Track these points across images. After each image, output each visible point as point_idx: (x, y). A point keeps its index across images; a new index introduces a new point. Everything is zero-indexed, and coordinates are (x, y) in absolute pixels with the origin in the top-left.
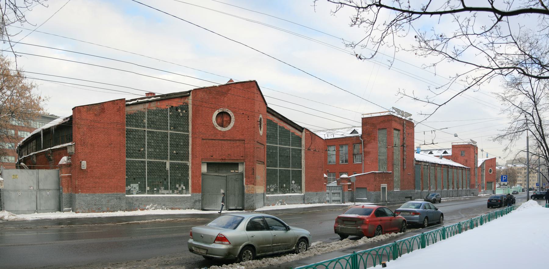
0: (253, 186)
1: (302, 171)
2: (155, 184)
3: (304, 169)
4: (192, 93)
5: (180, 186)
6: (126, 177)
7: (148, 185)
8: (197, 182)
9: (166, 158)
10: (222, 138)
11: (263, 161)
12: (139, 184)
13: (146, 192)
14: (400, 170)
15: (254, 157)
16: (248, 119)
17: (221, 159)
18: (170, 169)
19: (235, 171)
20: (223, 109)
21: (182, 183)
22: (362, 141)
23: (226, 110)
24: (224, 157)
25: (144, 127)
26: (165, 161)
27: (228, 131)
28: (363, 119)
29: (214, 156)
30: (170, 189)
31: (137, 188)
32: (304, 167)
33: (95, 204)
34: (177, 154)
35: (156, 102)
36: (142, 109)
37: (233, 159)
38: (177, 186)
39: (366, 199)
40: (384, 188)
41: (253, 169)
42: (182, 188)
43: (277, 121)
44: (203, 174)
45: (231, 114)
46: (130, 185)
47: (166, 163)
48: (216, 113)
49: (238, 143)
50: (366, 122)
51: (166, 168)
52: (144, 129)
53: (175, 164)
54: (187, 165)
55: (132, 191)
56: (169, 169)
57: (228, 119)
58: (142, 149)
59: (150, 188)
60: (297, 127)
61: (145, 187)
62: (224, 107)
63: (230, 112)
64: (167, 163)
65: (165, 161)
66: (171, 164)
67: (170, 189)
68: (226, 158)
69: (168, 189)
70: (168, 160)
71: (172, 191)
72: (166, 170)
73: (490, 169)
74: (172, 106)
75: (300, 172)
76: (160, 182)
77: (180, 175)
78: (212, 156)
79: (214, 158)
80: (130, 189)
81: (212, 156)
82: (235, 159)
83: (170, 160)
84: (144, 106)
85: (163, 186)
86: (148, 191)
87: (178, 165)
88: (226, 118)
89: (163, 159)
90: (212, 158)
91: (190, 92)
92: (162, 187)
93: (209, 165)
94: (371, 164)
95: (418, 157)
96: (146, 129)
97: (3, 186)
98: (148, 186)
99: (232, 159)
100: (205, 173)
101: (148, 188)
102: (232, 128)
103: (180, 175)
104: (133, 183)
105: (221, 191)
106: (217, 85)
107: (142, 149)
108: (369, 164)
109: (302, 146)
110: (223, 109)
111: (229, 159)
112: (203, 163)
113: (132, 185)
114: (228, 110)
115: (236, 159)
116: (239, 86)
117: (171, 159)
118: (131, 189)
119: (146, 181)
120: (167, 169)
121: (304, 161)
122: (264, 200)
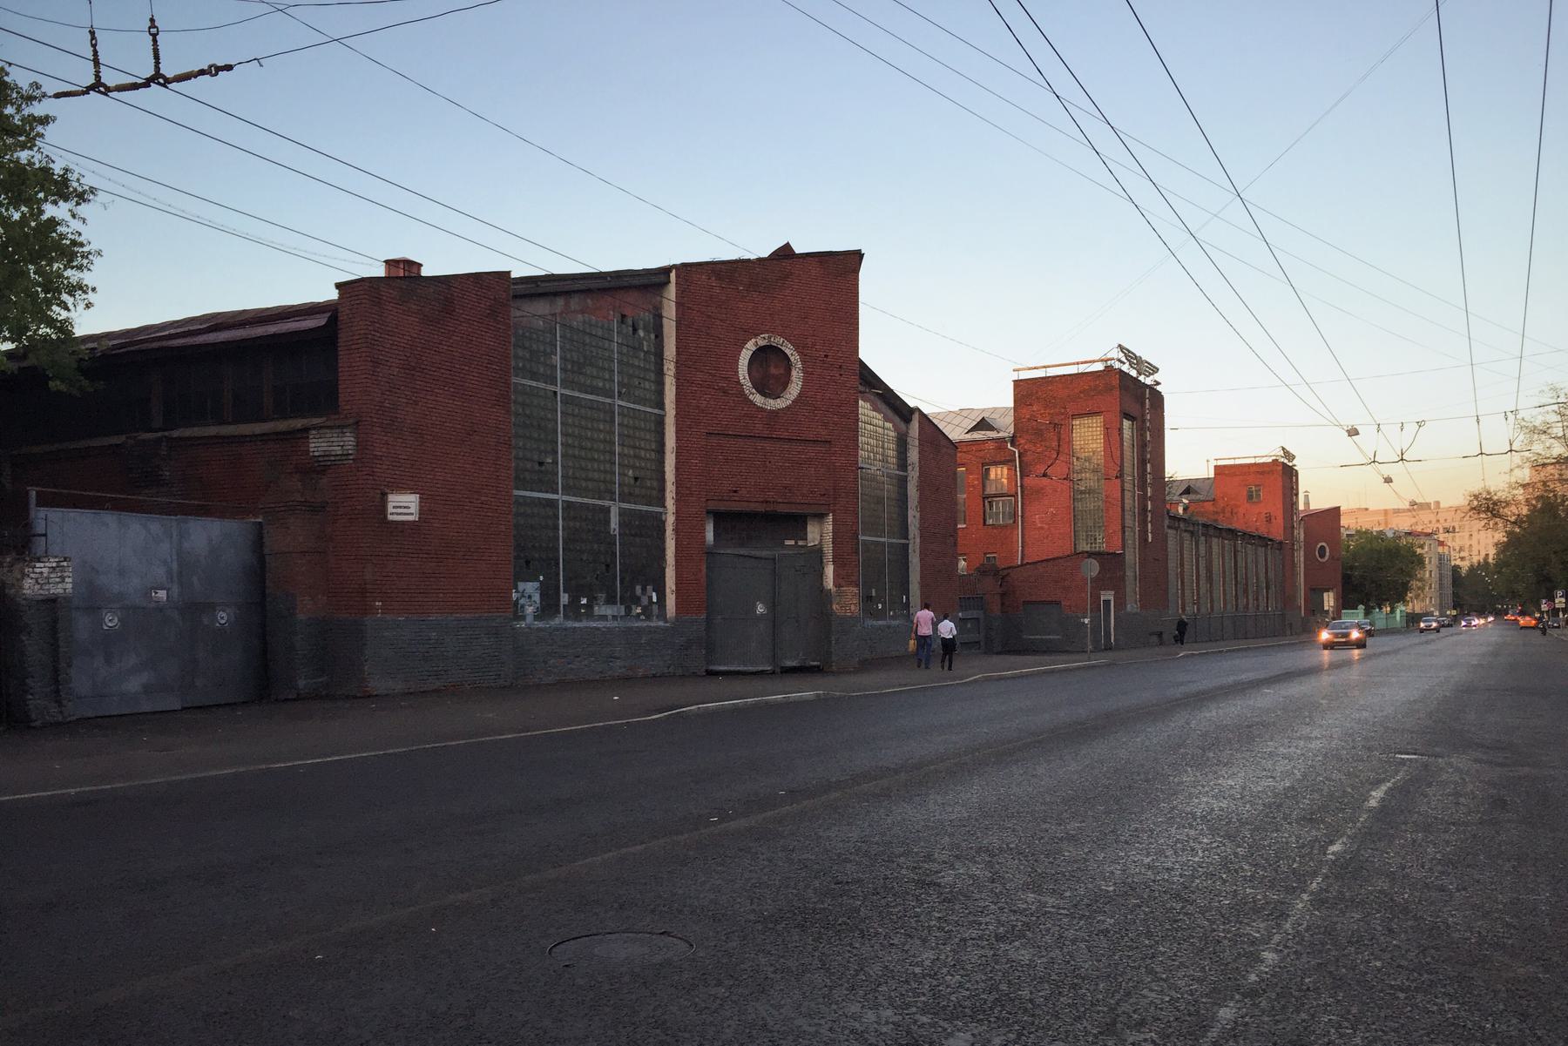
1: (910, 546)
3: (918, 540)
4: (677, 276)
5: (644, 590)
10: (766, 433)
14: (1137, 547)
17: (762, 502)
19: (796, 543)
20: (770, 337)
22: (1017, 455)
23: (778, 341)
25: (553, 381)
26: (607, 503)
28: (1017, 383)
29: (743, 492)
31: (537, 597)
32: (917, 533)
33: (426, 654)
40: (1107, 602)
44: (710, 553)
48: (750, 347)
50: (1026, 391)
52: (552, 388)
56: (617, 532)
57: (782, 371)
59: (569, 596)
62: (772, 331)
63: (789, 350)
65: (607, 503)
66: (622, 513)
67: (621, 604)
69: (614, 603)
73: (1322, 546)
78: (735, 492)
86: (564, 605)
88: (776, 367)
91: (666, 271)
94: (1046, 527)
95: (390, 518)
96: (559, 390)
97: (70, 586)
101: (564, 598)
106: (753, 257)
108: (1042, 528)
109: (910, 468)
110: (770, 337)
115: (806, 502)
118: (522, 601)
120: (612, 533)
121: (918, 515)
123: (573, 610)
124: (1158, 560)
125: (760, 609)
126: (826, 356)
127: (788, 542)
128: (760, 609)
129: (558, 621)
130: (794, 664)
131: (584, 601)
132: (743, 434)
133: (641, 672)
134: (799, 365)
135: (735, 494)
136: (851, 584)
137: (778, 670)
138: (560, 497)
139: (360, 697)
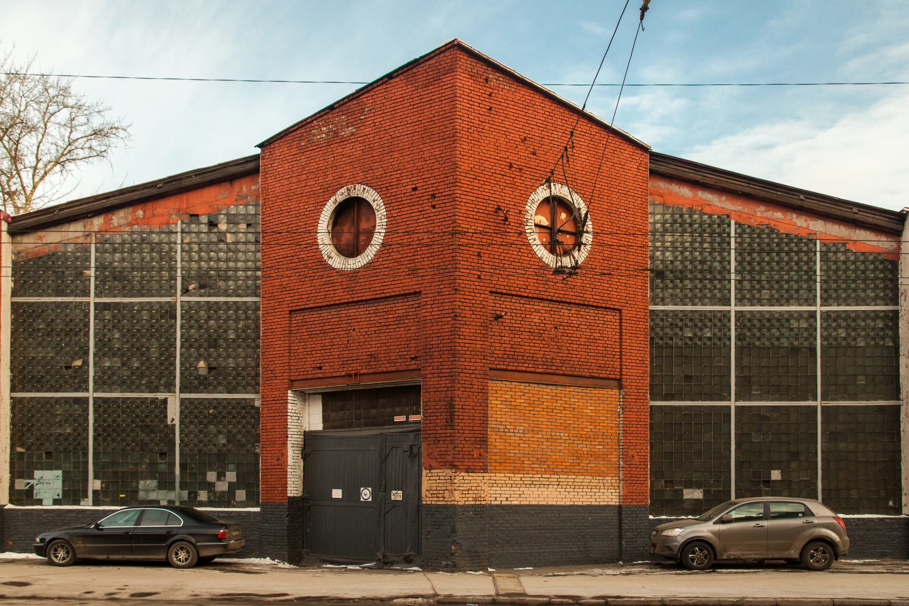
0: (449, 472)
2: (121, 469)
8: (276, 463)
9: (169, 387)
10: (346, 298)
11: (618, 377)
15: (454, 356)
16: (434, 207)
18: (181, 422)
19: (407, 418)
21: (231, 466)
24: (355, 367)
26: (161, 396)
29: (326, 368)
36: (78, 237)
37: (385, 370)
39: (257, 509)
41: (452, 406)
43: (740, 208)
47: (165, 401)
48: (329, 208)
49: (400, 307)
51: (166, 417)
53: (191, 401)
56: (177, 422)
58: (79, 363)
59: (102, 483)
60: (859, 217)
61: (86, 480)
64: (169, 402)
68: (362, 372)
72: (166, 426)
77: (222, 440)
78: (320, 368)
82: (390, 369)
83: (181, 392)
86: (95, 492)
87: (215, 408)
93: (330, 400)
99: (380, 370)
102: (378, 255)
103: (224, 441)
104: (42, 469)
107: (79, 363)
111: (371, 371)
112: (311, 396)
113: (38, 474)
115: (394, 369)
116: (398, 88)
119: (87, 462)
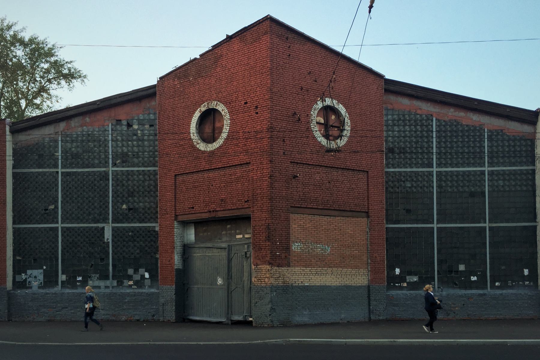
5: (136, 271)
6: (158, 256)
7: (62, 270)
11: (367, 211)
12: (44, 270)
13: (58, 285)
18: (113, 241)
20: (208, 104)
26: (100, 225)
27: (218, 148)
29: (196, 207)
30: (113, 279)
31: (41, 277)
34: (130, 209)
35: (81, 117)
37: (230, 208)
38: (130, 271)
39: (396, 285)
42: (143, 276)
45: (223, 110)
46: (25, 273)
47: (103, 228)
51: (104, 237)
52: (55, 170)
54: (155, 231)
55: (29, 282)
56: (110, 240)
58: (52, 207)
59: (67, 277)
61: (57, 275)
65: (100, 225)
67: (113, 279)
68: (217, 209)
70: (109, 223)
71: (118, 282)
72: (104, 243)
74: (117, 120)
75: (14, 223)
76: (90, 265)
79: (196, 212)
80: (26, 279)
81: (193, 208)
82: (233, 208)
83: (112, 223)
84: (55, 128)
85: (95, 273)
86: (62, 282)
89: (98, 222)
90: (193, 212)
92: (93, 275)
98: (63, 273)
100: (192, 245)
101: (62, 277)
105: (217, 281)
107: (52, 207)
111: (222, 209)
113: (29, 272)
114: (217, 103)
115: (235, 207)
117: (114, 221)
118: (28, 280)
122: (369, 302)
123: (71, 283)
124: (246, 202)
125: (220, 281)
126: (246, 103)
127: (239, 236)
128: (220, 281)
129: (58, 289)
130: (241, 318)
131: (80, 278)
132: (195, 171)
133: (124, 318)
134: (228, 116)
135: (192, 210)
136: (264, 263)
137: (230, 322)
138: (487, 225)
139: (369, 308)
